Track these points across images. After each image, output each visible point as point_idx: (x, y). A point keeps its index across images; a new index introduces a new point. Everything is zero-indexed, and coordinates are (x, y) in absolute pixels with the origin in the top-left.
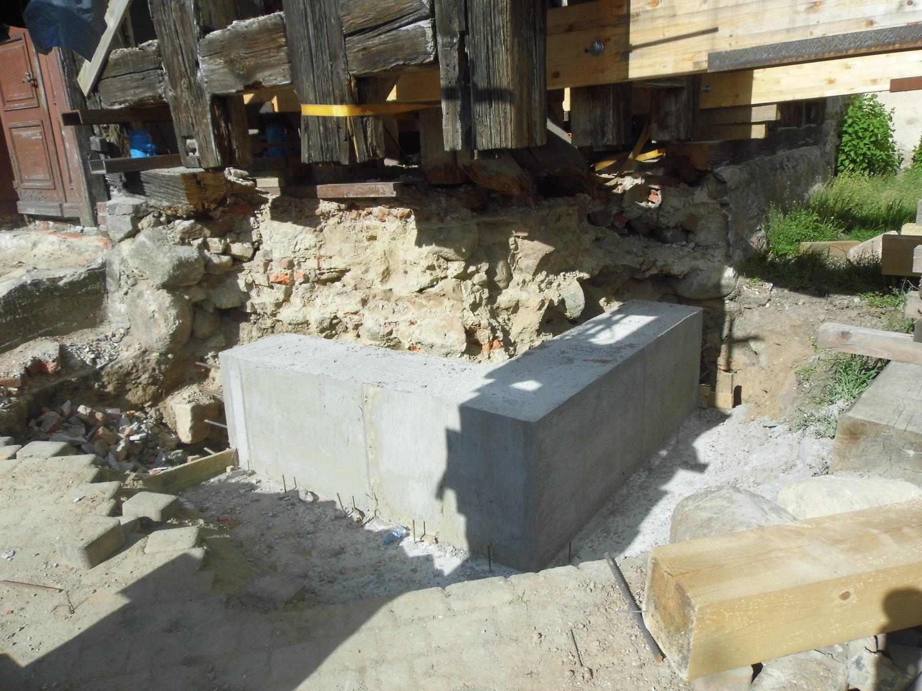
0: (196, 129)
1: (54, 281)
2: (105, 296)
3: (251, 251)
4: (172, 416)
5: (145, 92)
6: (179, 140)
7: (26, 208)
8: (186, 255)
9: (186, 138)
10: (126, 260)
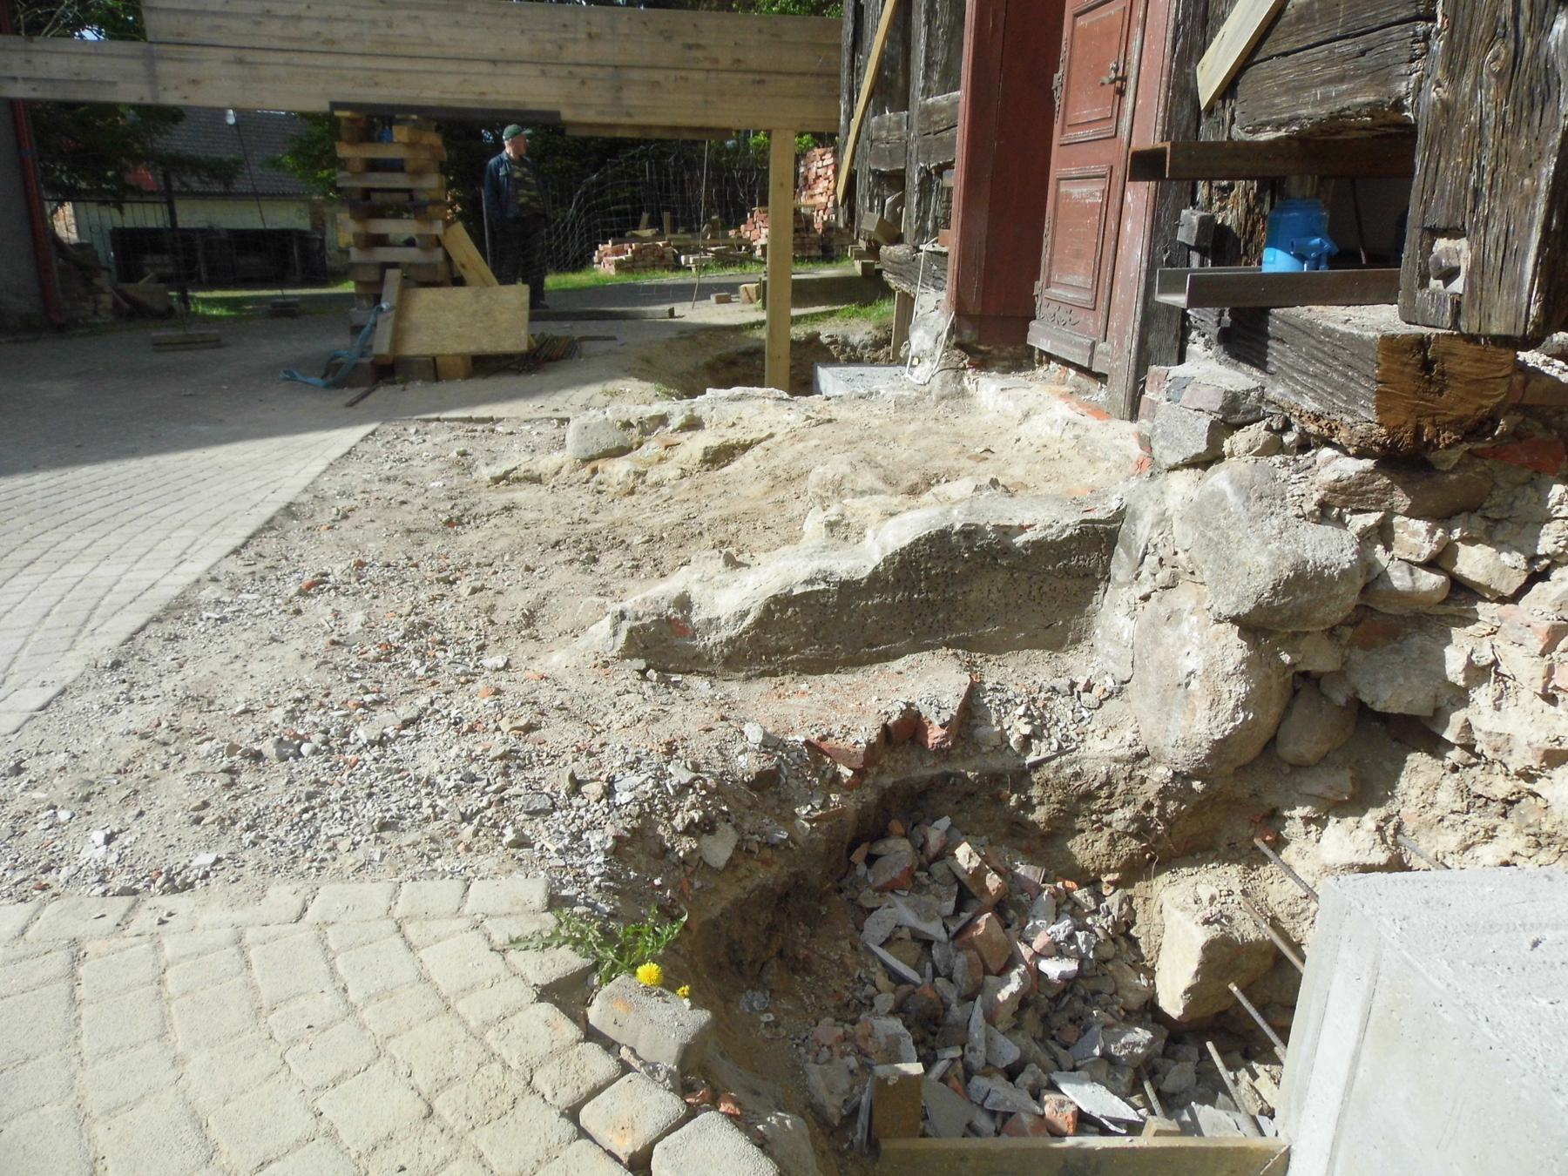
0: (1483, 209)
1: (1006, 531)
2: (1102, 585)
3: (1520, 580)
4: (1154, 930)
5: (1353, 92)
6: (1413, 234)
7: (1040, 337)
8: (1321, 555)
9: (1435, 233)
10: (1169, 519)
